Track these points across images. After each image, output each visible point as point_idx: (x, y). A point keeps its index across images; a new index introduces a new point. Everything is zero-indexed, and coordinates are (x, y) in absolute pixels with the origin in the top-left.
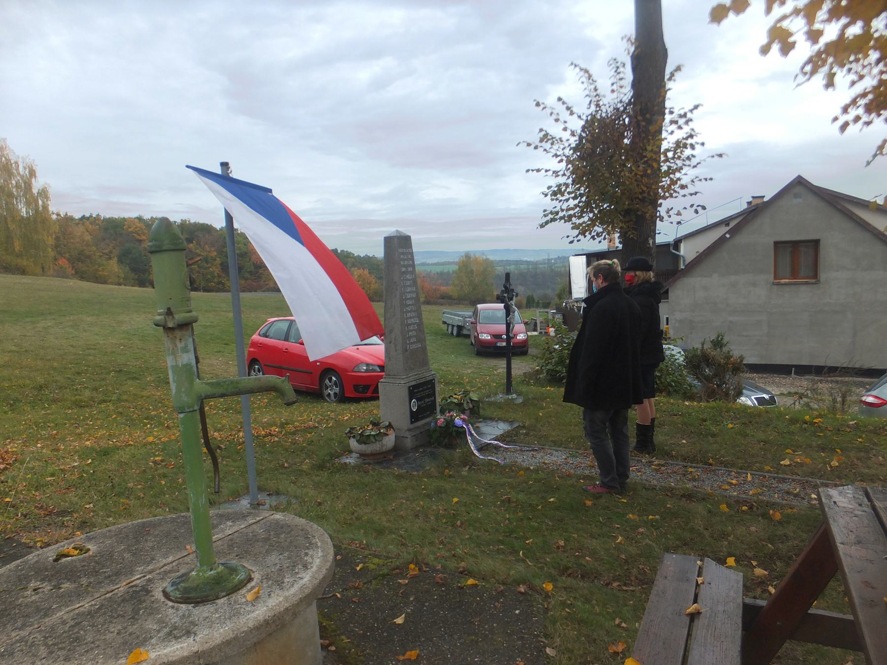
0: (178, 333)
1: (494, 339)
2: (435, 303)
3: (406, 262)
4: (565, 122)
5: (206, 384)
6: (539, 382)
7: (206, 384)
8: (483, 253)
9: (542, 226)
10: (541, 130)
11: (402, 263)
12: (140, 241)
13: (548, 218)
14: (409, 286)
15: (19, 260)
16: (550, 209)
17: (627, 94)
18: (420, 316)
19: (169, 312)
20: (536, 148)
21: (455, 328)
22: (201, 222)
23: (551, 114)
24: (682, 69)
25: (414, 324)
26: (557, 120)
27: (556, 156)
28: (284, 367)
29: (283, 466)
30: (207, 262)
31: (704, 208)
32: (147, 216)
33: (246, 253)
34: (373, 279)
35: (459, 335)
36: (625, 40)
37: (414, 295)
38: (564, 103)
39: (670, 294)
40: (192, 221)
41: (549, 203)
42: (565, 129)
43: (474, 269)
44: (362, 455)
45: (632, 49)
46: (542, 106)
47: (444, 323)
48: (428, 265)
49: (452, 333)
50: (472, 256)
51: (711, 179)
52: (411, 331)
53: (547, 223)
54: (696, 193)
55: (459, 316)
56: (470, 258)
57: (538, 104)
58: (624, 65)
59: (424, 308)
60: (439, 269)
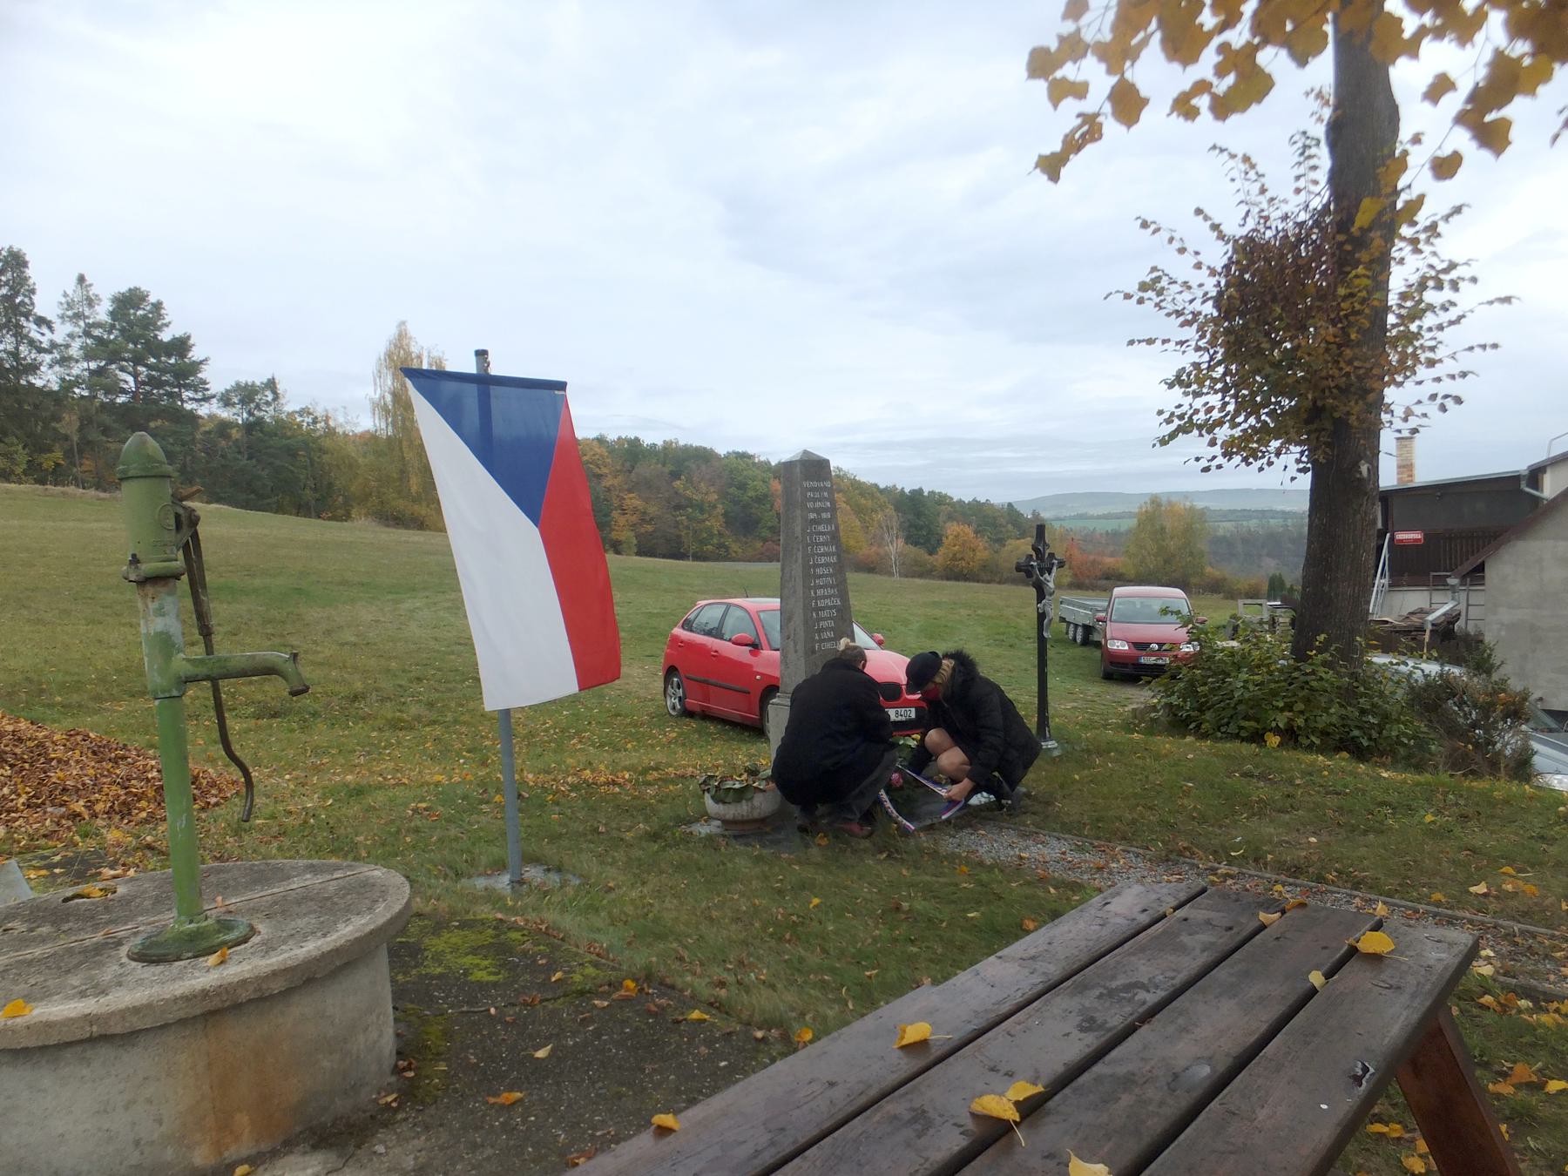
0: (150, 590)
1: (1136, 652)
2: (1093, 588)
3: (818, 504)
4: (1197, 253)
5: (188, 660)
6: (1152, 728)
7: (188, 660)
8: (1186, 495)
9: (1163, 442)
10: (1154, 269)
11: (810, 505)
12: (599, 477)
13: (1173, 427)
14: (823, 544)
15: (416, 507)
16: (1169, 408)
17: (1320, 196)
18: (844, 596)
19: (135, 561)
20: (1141, 301)
21: (1080, 630)
22: (696, 444)
23: (1171, 240)
24: (1423, 138)
25: (831, 608)
26: (1182, 251)
27: (1179, 313)
28: (712, 680)
29: (595, 830)
30: (702, 511)
31: (1458, 400)
32: (612, 436)
33: (766, 496)
34: (981, 543)
35: (1086, 642)
36: (1312, 96)
37: (834, 560)
38: (1206, 218)
39: (1490, 573)
40: (682, 443)
41: (1176, 398)
42: (1198, 266)
43: (1168, 525)
44: (726, 823)
45: (1327, 113)
46: (1153, 227)
47: (1063, 620)
48: (1092, 517)
49: (1075, 639)
50: (1164, 500)
51: (1495, 346)
52: (825, 619)
53: (1173, 436)
54: (1464, 375)
55: (1085, 607)
56: (1159, 505)
57: (1145, 225)
58: (1318, 142)
59: (853, 577)
60: (1110, 526)
